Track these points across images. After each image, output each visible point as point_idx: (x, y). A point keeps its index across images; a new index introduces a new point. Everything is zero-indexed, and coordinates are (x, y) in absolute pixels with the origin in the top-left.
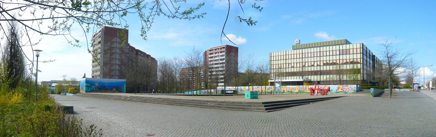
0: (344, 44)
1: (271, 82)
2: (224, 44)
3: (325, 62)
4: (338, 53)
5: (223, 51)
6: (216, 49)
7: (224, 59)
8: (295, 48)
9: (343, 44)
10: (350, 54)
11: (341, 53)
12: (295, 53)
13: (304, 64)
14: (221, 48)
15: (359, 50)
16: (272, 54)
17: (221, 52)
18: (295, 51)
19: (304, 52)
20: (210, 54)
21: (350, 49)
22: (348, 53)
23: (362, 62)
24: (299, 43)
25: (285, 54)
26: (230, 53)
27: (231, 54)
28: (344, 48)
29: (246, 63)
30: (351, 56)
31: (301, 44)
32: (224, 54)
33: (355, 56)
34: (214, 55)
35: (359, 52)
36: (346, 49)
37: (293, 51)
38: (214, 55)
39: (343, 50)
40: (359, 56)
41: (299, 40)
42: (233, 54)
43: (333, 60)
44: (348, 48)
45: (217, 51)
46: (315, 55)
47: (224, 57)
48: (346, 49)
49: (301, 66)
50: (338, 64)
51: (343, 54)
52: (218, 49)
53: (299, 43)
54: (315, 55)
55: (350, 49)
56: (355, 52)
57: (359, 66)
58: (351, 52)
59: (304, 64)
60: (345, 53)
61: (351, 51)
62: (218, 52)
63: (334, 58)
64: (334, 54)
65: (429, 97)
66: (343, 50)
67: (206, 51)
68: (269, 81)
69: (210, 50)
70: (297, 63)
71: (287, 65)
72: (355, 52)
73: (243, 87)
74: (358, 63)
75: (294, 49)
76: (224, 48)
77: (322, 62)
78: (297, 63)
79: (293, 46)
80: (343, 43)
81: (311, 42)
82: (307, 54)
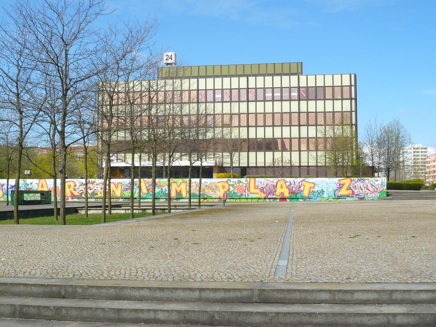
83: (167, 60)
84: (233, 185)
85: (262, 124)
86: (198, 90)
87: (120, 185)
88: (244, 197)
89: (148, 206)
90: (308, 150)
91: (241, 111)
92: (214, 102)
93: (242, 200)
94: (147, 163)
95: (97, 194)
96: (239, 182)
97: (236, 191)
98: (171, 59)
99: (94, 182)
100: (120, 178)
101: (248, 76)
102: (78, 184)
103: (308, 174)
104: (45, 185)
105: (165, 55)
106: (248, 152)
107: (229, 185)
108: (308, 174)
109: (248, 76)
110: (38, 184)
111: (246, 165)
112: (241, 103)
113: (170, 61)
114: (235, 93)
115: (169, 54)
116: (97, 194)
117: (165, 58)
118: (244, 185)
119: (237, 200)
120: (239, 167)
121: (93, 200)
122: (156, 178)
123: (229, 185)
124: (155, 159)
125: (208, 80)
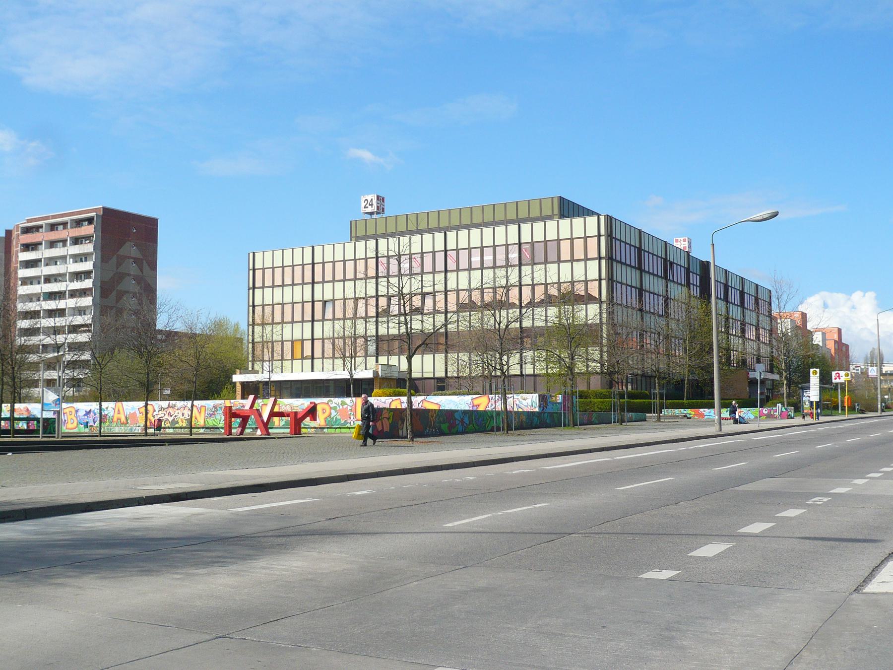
0: (550, 218)
1: (244, 385)
2: (92, 203)
3: (464, 296)
4: (514, 256)
5: (88, 238)
6: (53, 227)
7: (87, 274)
8: (361, 232)
9: (544, 218)
10: (559, 261)
11: (527, 255)
12: (488, 241)
13: (383, 302)
14: (79, 223)
15: (592, 243)
16: (259, 256)
17: (76, 241)
18: (361, 244)
19: (451, 245)
20: (27, 247)
21: (558, 241)
22: (552, 256)
23: (604, 298)
24: (380, 210)
25: (308, 260)
26: (121, 245)
27: (123, 251)
28: (539, 237)
29: (189, 294)
30: (565, 268)
31: (386, 214)
32: (88, 248)
33: (579, 267)
34: (44, 253)
35: (593, 253)
36: (545, 242)
37: (350, 246)
38: (44, 253)
39: (533, 243)
40: (593, 274)
41: (380, 199)
42: (131, 250)
43: (572, 283)
44: (552, 235)
45: (61, 234)
46: (428, 267)
47: (88, 266)
48: (545, 242)
49: (372, 312)
50: (513, 306)
51: (533, 263)
52: (65, 224)
53: (380, 210)
54: (428, 267)
55: (558, 241)
56: (579, 254)
57: (593, 309)
58: (565, 255)
59: (383, 302)
60: (539, 257)
61: (565, 246)
62: (64, 242)
63: (579, 275)
64: (501, 260)
65: (464, 394)
66: (533, 243)
67: (9, 233)
68: (237, 378)
69: (27, 230)
70: (356, 300)
71: (318, 306)
72: (579, 254)
73: (111, 405)
74: (588, 299)
75: (359, 238)
76: (90, 221)
77: (452, 298)
78: (356, 300)
79: (353, 225)
80: (547, 211)
81: (433, 208)
82: (464, 255)
83: (365, 207)
84: (335, 408)
85: (341, 316)
86: (520, 244)
87: (203, 409)
88: (348, 425)
89: (150, 440)
90: (366, 356)
91: (347, 296)
92: (470, 269)
93: (343, 431)
94: (341, 374)
95: (177, 422)
96: (343, 403)
97: (339, 417)
98: (372, 205)
99: (175, 406)
100: (214, 399)
101: (445, 231)
102: (157, 409)
103: (522, 388)
104: (121, 411)
105: (363, 199)
106: (447, 352)
107: (331, 408)
108: (522, 388)
109: (445, 231)
110: (114, 409)
111: (443, 375)
112: (574, 263)
113: (370, 209)
114: (579, 244)
115: (369, 198)
116: (177, 422)
117: (363, 204)
118: (349, 408)
119: (338, 431)
120: (434, 378)
121: (171, 431)
122: (411, 395)
123: (331, 408)
124: (353, 367)
125: (535, 225)
